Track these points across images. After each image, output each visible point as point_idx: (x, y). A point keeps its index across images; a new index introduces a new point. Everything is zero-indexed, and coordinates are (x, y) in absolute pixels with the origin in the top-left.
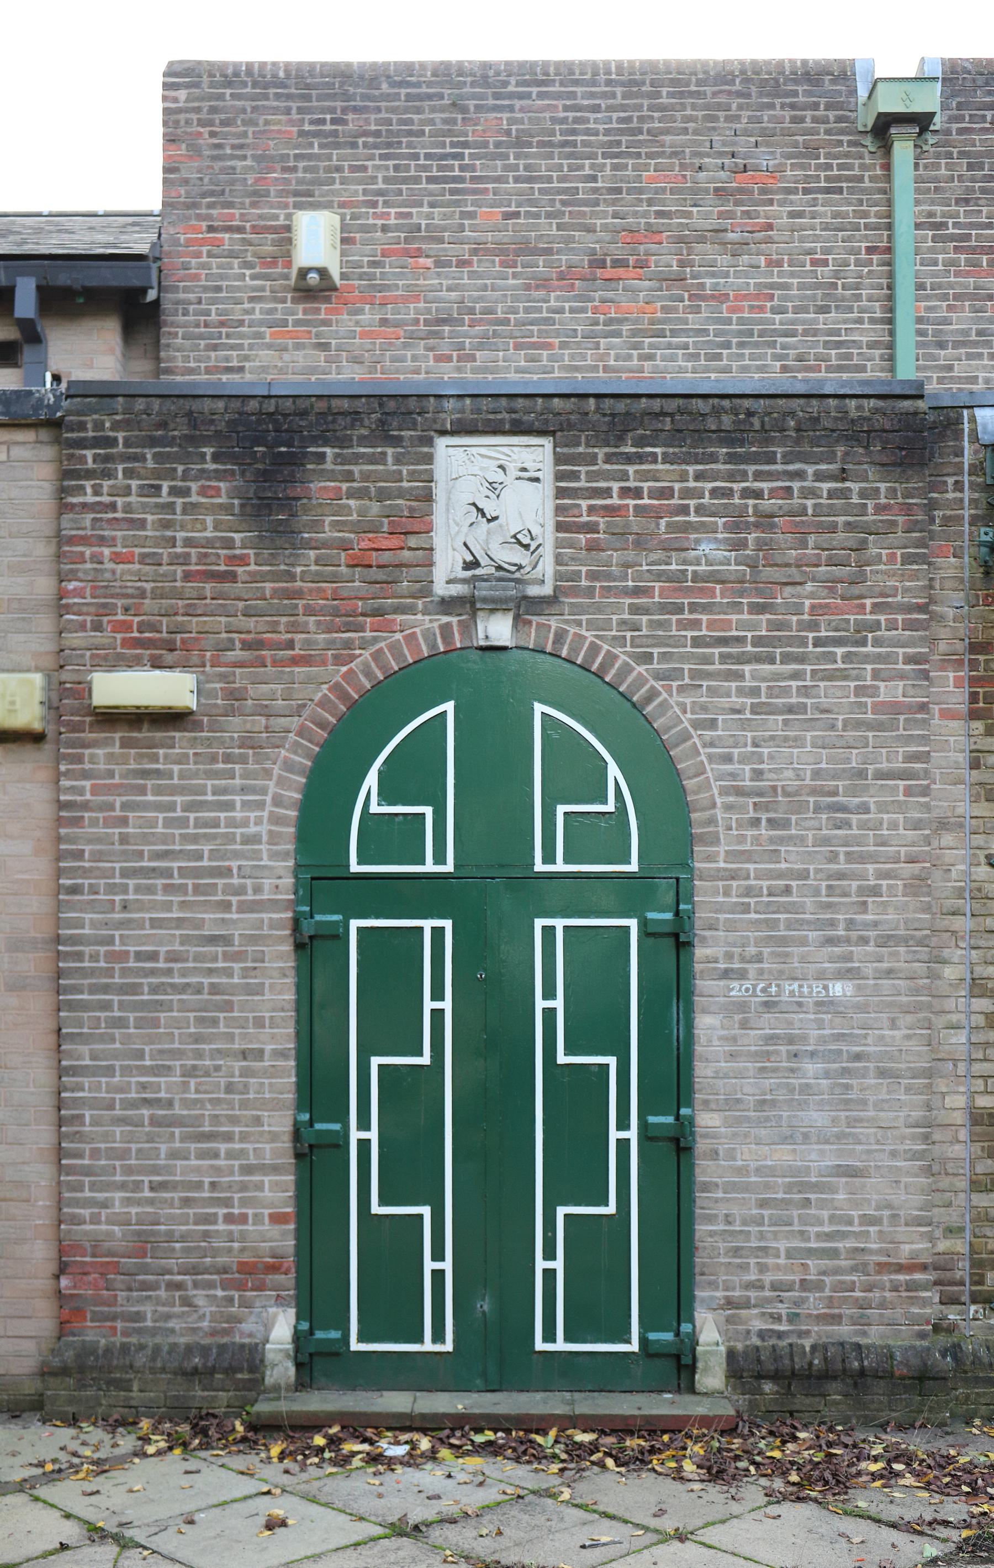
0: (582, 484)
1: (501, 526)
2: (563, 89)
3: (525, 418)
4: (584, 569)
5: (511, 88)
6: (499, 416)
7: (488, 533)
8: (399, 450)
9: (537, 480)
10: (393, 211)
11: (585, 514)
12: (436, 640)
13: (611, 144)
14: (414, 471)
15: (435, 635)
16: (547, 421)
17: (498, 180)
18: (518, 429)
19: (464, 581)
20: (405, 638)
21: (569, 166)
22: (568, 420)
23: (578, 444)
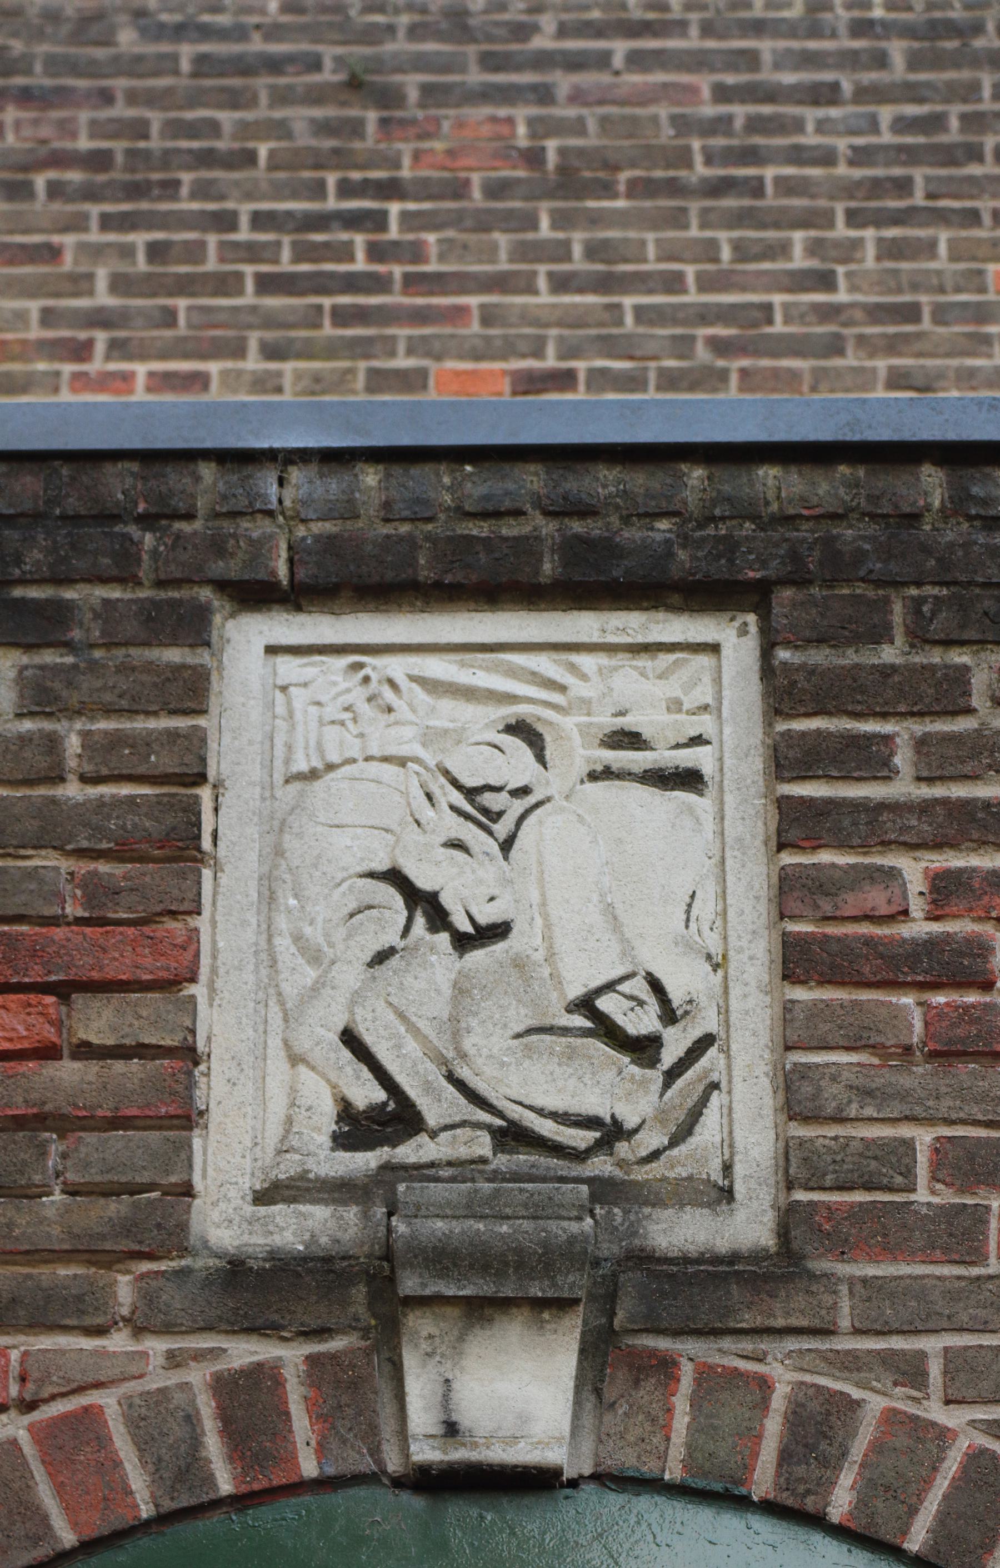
0: (903, 788)
1: (519, 964)
2: (711, 44)
3: (632, 534)
4: (924, 1137)
5: (540, 42)
6: (510, 529)
7: (461, 990)
8: (49, 657)
9: (689, 779)
10: (141, 369)
11: (917, 907)
12: (196, 1442)
13: (876, 187)
14: (116, 741)
15: (191, 1419)
16: (729, 546)
17: (500, 283)
18: (596, 580)
19: (339, 1190)
20: (45, 1436)
21: (739, 248)
22: (828, 542)
23: (881, 635)
